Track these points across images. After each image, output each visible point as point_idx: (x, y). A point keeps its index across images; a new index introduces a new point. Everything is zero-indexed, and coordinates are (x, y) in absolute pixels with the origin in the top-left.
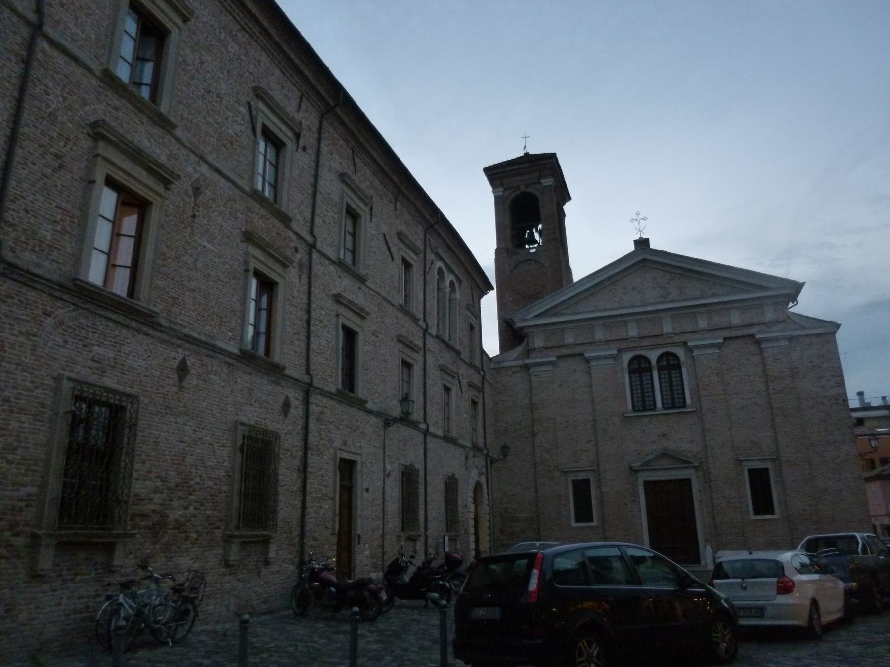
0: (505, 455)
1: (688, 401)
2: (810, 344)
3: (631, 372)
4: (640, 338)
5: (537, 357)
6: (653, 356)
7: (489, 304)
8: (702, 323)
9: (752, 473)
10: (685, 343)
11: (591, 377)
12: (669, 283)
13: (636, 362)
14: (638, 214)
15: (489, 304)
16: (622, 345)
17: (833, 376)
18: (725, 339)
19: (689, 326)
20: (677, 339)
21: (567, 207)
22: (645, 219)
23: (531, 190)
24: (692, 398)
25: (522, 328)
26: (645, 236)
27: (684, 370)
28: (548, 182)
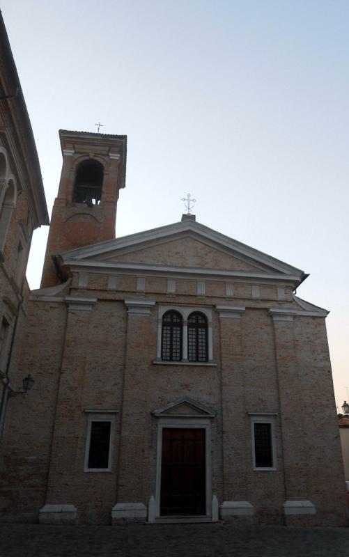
0: (26, 388)
1: (211, 357)
2: (308, 324)
3: (164, 324)
4: (177, 295)
5: (78, 296)
6: (186, 313)
7: (40, 237)
8: (230, 292)
9: (258, 426)
10: (214, 306)
11: (127, 323)
12: (206, 255)
13: (194, 317)
14: (189, 195)
15: (40, 237)
16: (160, 299)
17: (323, 352)
18: (246, 308)
19: (218, 293)
20: (208, 301)
21: (121, 191)
22: (194, 200)
23: (99, 159)
24: (214, 355)
25: (69, 267)
26: (192, 213)
27: (210, 329)
28: (115, 156)
